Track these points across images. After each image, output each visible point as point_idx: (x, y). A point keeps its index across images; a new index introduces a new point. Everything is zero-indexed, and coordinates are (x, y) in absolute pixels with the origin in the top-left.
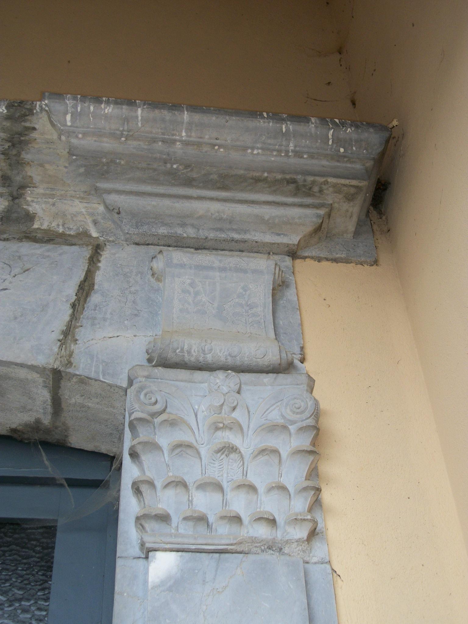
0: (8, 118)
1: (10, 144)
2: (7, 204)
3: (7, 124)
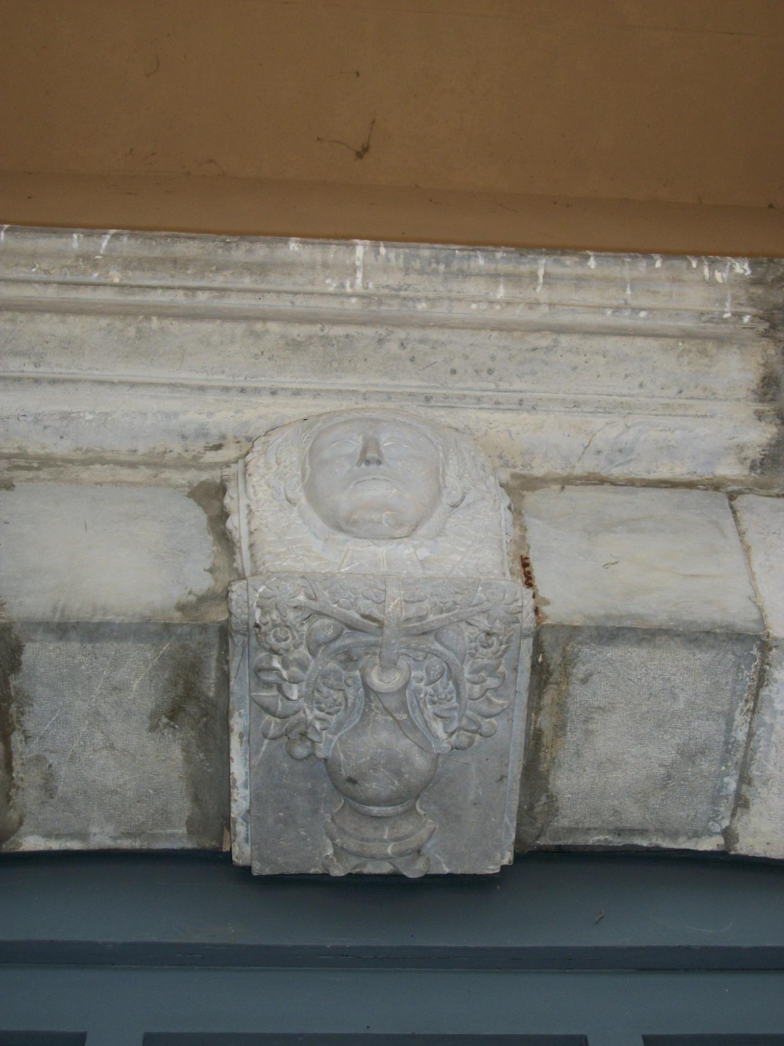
0: (756, 282)
1: (767, 325)
2: (774, 430)
3: (759, 291)
